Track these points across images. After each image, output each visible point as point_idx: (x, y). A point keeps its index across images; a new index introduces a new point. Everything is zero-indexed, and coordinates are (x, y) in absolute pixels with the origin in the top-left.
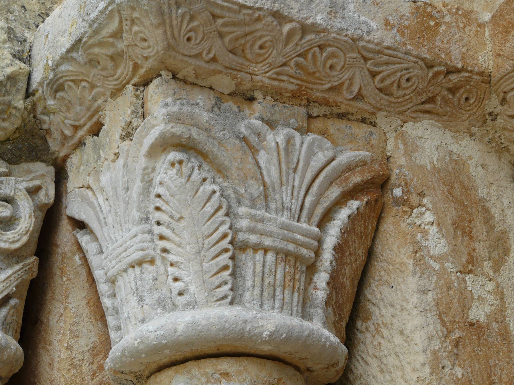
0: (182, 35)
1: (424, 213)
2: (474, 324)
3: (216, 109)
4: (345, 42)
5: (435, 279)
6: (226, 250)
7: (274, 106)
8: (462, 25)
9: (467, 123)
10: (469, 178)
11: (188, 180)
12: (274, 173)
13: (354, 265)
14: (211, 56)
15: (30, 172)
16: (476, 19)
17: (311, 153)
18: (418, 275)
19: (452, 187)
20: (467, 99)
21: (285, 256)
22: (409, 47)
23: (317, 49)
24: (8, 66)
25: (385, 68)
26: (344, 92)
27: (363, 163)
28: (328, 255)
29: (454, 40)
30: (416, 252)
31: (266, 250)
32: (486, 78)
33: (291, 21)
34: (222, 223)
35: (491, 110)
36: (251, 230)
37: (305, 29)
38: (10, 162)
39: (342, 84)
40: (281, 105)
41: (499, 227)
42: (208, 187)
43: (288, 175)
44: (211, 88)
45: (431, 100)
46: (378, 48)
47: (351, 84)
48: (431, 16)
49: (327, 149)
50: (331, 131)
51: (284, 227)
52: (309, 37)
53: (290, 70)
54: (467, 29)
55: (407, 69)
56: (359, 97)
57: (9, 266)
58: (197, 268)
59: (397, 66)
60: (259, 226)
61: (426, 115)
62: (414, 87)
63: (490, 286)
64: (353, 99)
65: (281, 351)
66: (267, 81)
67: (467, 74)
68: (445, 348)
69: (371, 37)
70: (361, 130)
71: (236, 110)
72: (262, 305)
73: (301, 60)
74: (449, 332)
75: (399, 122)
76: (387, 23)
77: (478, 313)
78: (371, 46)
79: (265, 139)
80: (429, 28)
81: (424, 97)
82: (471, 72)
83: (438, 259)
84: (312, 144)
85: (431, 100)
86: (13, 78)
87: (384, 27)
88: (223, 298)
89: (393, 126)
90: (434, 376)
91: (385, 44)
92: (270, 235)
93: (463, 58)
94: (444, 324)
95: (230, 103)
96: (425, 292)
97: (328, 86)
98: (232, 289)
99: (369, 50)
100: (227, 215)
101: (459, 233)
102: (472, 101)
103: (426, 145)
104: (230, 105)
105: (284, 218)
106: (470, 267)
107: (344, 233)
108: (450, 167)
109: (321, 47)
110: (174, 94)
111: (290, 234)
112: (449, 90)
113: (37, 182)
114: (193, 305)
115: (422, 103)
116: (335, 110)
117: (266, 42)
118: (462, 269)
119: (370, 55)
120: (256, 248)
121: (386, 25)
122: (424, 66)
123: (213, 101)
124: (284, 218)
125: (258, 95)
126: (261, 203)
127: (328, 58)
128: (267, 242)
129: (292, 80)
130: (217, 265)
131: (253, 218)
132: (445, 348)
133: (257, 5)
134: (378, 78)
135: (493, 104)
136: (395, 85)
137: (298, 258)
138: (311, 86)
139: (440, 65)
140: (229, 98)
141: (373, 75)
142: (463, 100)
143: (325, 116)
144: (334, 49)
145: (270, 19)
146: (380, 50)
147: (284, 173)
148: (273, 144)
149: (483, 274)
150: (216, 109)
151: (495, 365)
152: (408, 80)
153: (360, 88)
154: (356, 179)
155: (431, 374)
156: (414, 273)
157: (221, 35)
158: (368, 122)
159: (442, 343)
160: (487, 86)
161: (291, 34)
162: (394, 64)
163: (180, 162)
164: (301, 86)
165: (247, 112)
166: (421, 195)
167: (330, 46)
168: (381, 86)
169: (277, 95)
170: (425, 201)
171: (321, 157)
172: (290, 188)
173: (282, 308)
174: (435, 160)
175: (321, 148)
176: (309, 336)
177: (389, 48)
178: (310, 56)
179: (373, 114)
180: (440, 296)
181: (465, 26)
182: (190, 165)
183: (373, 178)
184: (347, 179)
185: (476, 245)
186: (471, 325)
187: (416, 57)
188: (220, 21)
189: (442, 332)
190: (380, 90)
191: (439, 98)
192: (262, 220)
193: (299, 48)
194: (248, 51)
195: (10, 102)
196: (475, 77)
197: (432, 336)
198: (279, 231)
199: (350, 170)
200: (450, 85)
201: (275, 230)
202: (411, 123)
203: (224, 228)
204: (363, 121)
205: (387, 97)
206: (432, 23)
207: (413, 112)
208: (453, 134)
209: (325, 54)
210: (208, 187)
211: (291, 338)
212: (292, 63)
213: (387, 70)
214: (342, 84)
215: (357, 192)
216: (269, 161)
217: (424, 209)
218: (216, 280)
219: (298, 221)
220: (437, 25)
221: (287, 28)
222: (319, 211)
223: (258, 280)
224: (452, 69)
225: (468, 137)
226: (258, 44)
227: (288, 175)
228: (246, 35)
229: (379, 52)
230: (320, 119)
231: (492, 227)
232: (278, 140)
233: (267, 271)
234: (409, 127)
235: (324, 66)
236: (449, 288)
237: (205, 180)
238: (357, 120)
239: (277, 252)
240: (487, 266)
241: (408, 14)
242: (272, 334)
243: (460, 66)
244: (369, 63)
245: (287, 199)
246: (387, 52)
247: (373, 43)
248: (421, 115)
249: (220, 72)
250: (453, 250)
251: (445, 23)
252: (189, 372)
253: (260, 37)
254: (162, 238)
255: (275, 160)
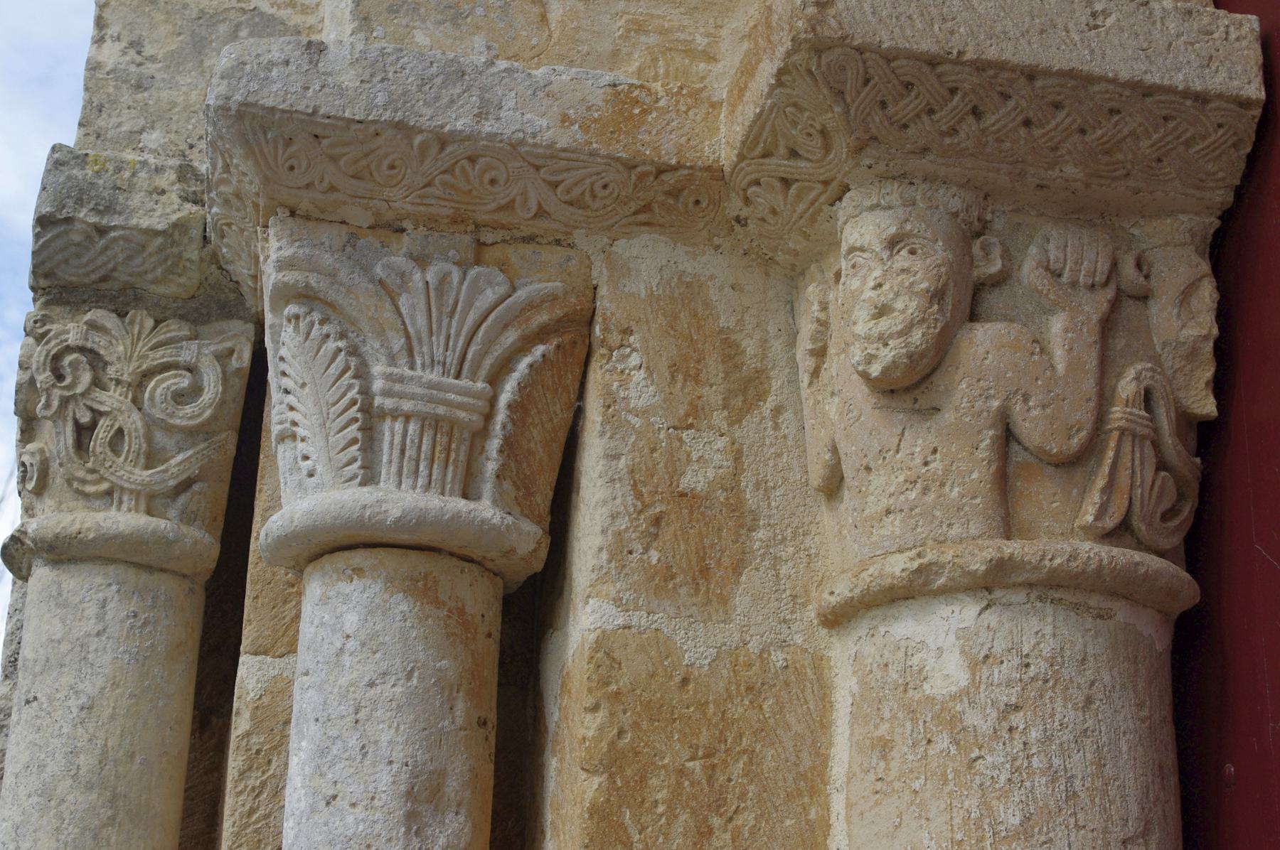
0: (280, 162)
1: (629, 355)
2: (686, 495)
3: (349, 249)
4: (501, 149)
5: (633, 439)
6: (356, 420)
7: (426, 237)
8: (684, 108)
9: (705, 233)
10: (707, 305)
11: (307, 338)
12: (421, 320)
13: (548, 426)
14: (325, 184)
15: (222, 332)
16: (709, 98)
17: (475, 291)
18: (608, 435)
19: (676, 317)
20: (697, 202)
21: (433, 423)
22: (595, 146)
23: (465, 162)
24: (174, 212)
25: (565, 175)
26: (519, 211)
27: (553, 298)
28: (501, 416)
29: (669, 128)
30: (609, 407)
31: (407, 418)
32: (715, 172)
33: (421, 131)
34: (350, 387)
35: (736, 214)
36: (387, 393)
37: (443, 140)
38: (195, 322)
39: (513, 201)
40: (437, 234)
41: (751, 364)
42: (331, 345)
43: (440, 322)
44: (343, 222)
45: (647, 208)
46: (549, 152)
47: (526, 201)
48: (637, 102)
49: (499, 284)
50: (513, 260)
51: (431, 386)
52: (449, 149)
53: (437, 190)
54: (691, 113)
55: (598, 174)
56: (541, 213)
57: (193, 445)
58: (322, 443)
59: (582, 172)
60: (397, 387)
61: (643, 228)
62: (615, 195)
63: (721, 443)
64: (535, 216)
65: (424, 538)
66: (409, 207)
67: (686, 172)
68: (638, 526)
69: (538, 140)
70: (553, 256)
71: (379, 245)
72: (400, 484)
73: (447, 177)
74: (646, 507)
75: (605, 240)
76: (565, 119)
77: (693, 480)
78: (540, 151)
79: (411, 280)
80: (632, 116)
81: (633, 206)
82: (691, 168)
83: (643, 413)
84: (477, 278)
85: (647, 208)
86: (183, 225)
87: (559, 124)
88: (351, 479)
89: (599, 247)
90: (613, 565)
91: (558, 146)
92: (413, 397)
93: (680, 152)
94: (639, 496)
95: (370, 238)
96: (616, 457)
97: (493, 206)
98: (362, 467)
99: (538, 156)
100: (355, 377)
101: (680, 377)
102: (704, 205)
103: (643, 267)
104: (368, 241)
105: (434, 376)
106: (690, 421)
107: (525, 387)
108: (677, 292)
109: (472, 160)
110: (291, 235)
111: (441, 395)
112: (669, 194)
113: (228, 344)
114: (320, 487)
115: (635, 213)
116: (518, 234)
117: (394, 160)
118: (677, 424)
119: (541, 162)
120: (395, 414)
121: (563, 121)
122: (621, 169)
123: (345, 238)
124: (434, 376)
125: (407, 224)
126: (403, 360)
127: (484, 171)
128: (407, 406)
129: (443, 203)
130: (344, 438)
131: (389, 377)
132: (638, 526)
133: (371, 118)
134: (560, 189)
135: (734, 206)
136: (587, 195)
137: (453, 424)
138: (470, 207)
139: (644, 163)
140: (369, 231)
141: (555, 185)
142: (691, 206)
143: (504, 241)
144: (488, 159)
145: (390, 132)
146: (553, 153)
147: (434, 320)
148: (421, 285)
149: (711, 427)
150: (349, 249)
151: (712, 546)
152: (605, 187)
153: (539, 204)
154: (542, 318)
155: (609, 561)
156: (602, 434)
157: (334, 159)
158: (565, 243)
159: (631, 521)
160: (720, 183)
161: (424, 148)
162: (578, 169)
163: (297, 317)
164: (459, 209)
165: (395, 246)
166: (627, 332)
167: (482, 156)
168: (567, 198)
169: (432, 223)
170: (632, 339)
171: (490, 296)
172: (442, 338)
173: (427, 487)
174: (654, 285)
175: (489, 283)
176: (452, 519)
177: (564, 150)
178: (457, 171)
179: (567, 233)
180: (637, 460)
181: (689, 109)
182: (308, 319)
183: (566, 315)
184: (528, 319)
185: (705, 391)
186: (682, 495)
187: (608, 156)
188: (325, 142)
189: (635, 506)
190: (571, 203)
191: (655, 206)
192: (401, 380)
193: (440, 163)
194: (375, 174)
195: (180, 253)
196: (699, 174)
197: (618, 513)
198: (426, 391)
199: (533, 307)
200: (667, 188)
201: (419, 390)
202: (624, 241)
203: (353, 394)
204: (558, 242)
205: (580, 211)
206: (637, 111)
207: (624, 225)
208: (687, 249)
209: (477, 167)
210: (331, 345)
211: (421, 521)
212: (437, 182)
213: (569, 178)
214: (513, 201)
215: (548, 334)
216: (413, 307)
217: (628, 350)
218: (345, 457)
219: (458, 376)
220: (645, 112)
221: (418, 140)
222: (488, 363)
223: (396, 453)
224: (664, 167)
225: (712, 251)
226: (385, 164)
227: (440, 322)
228: (366, 155)
229: (552, 157)
230: (499, 246)
231: (738, 367)
232: (428, 279)
233: (408, 442)
234: (620, 246)
235: (481, 182)
236: (653, 450)
237: (328, 336)
238: (549, 243)
239: (423, 419)
240: (719, 418)
241: (600, 103)
242: (398, 520)
243: (674, 162)
244: (543, 171)
245: (439, 352)
246: (563, 155)
247: (541, 146)
248: (635, 228)
249: (345, 203)
250: (665, 401)
251: (656, 109)
252: (322, 568)
253: (386, 156)
254: (292, 408)
255: (422, 305)
